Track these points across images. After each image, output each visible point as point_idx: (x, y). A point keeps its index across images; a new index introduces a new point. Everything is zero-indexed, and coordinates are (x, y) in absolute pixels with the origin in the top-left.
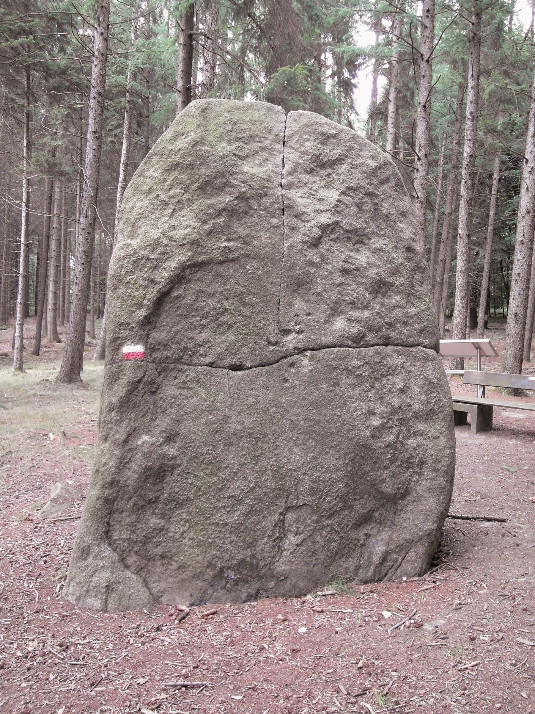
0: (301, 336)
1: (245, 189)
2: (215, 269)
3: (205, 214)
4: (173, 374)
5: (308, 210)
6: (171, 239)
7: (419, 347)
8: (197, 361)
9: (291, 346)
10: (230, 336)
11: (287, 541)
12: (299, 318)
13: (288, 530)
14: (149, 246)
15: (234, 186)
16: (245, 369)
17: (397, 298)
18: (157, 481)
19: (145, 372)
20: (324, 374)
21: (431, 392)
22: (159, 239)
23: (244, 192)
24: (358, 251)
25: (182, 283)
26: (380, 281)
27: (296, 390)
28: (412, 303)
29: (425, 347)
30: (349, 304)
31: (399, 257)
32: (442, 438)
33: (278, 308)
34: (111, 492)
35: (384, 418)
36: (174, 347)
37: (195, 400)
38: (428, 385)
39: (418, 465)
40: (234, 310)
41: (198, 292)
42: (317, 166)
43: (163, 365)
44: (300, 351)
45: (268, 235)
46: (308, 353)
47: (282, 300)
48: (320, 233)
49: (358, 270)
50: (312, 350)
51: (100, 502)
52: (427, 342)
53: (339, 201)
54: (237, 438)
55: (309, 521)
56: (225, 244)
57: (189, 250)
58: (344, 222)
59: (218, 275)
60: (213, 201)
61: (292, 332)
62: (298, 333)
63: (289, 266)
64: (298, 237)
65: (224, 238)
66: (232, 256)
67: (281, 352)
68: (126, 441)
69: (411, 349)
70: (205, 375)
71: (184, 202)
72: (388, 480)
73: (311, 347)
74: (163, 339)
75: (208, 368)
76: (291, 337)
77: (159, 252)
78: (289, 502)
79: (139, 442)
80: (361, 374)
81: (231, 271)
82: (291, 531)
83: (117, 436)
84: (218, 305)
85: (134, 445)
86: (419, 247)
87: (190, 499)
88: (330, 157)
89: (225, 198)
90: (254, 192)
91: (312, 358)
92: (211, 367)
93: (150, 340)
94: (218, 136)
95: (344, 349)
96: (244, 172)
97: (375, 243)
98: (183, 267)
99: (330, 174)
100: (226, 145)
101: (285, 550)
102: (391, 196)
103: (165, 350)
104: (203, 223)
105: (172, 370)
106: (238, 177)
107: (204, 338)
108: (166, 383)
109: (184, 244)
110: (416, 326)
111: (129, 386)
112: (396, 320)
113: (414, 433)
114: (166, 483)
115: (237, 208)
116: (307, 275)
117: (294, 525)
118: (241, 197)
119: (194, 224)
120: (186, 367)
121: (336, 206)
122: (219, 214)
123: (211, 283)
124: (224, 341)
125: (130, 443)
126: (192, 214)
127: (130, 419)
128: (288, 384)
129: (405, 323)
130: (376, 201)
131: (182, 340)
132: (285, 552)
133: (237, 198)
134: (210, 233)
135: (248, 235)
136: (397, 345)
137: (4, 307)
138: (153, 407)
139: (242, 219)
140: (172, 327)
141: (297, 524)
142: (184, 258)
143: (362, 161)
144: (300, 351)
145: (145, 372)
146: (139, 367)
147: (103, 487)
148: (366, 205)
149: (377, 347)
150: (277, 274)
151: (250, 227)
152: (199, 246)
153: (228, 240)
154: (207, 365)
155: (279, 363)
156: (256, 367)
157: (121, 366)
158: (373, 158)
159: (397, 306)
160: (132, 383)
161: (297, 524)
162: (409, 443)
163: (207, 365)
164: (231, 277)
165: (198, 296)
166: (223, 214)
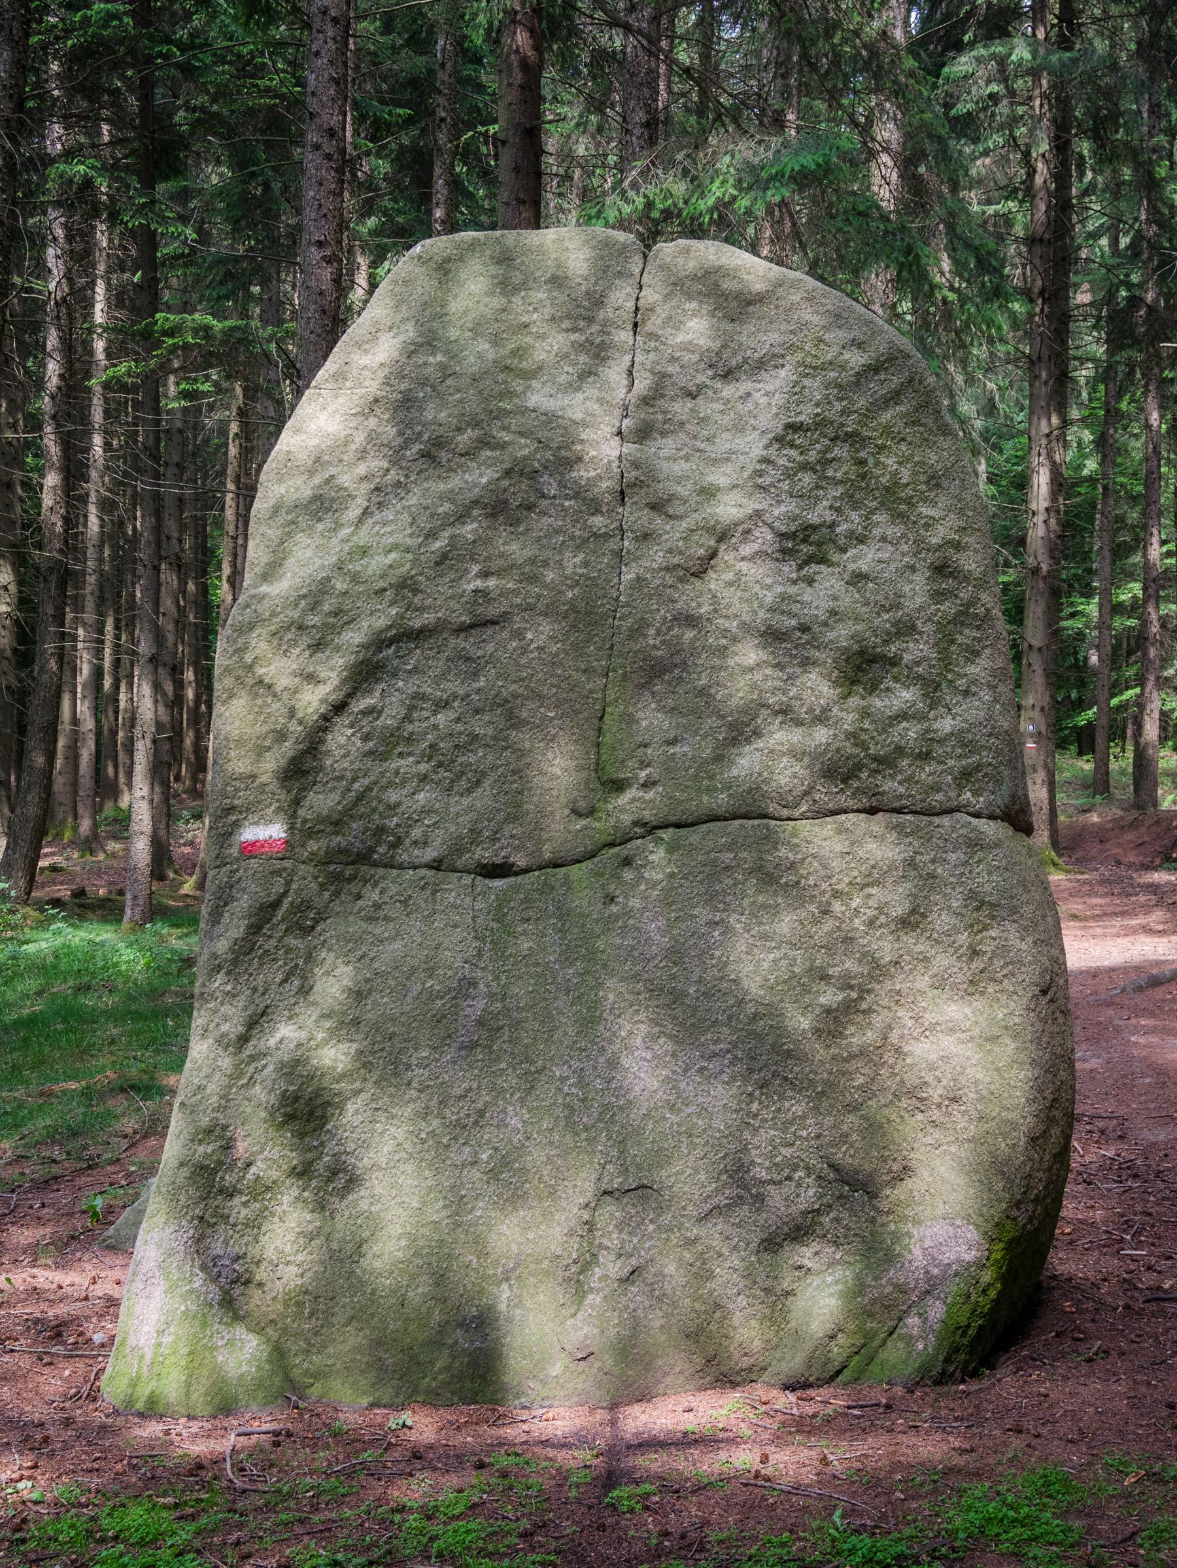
0: (650, 795)
1: (526, 452)
2: (452, 642)
3: (432, 515)
4: (354, 887)
5: (683, 490)
6: (355, 578)
7: (958, 815)
8: (405, 857)
9: (626, 819)
10: (482, 799)
11: (597, 1270)
12: (649, 751)
13: (601, 1246)
14: (304, 596)
15: (503, 446)
16: (516, 874)
17: (905, 696)
18: (309, 1128)
19: (288, 883)
20: (701, 882)
21: (985, 928)
22: (329, 579)
23: (525, 458)
24: (810, 582)
25: (377, 680)
26: (861, 653)
27: (631, 922)
28: (946, 706)
29: (977, 815)
30: (777, 713)
31: (916, 590)
32: (1008, 1041)
33: (600, 730)
34: (209, 1151)
35: (852, 987)
36: (354, 826)
37: (397, 945)
38: (978, 909)
39: (939, 1106)
40: (494, 738)
41: (413, 698)
42: (713, 378)
43: (332, 867)
44: (650, 829)
45: (581, 556)
46: (666, 834)
47: (608, 710)
48: (712, 543)
49: (804, 628)
50: (678, 826)
51: (185, 1172)
52: (980, 803)
53: (766, 460)
54: (489, 1030)
55: (651, 1227)
56: (479, 583)
57: (392, 603)
58: (776, 513)
59: (460, 658)
60: (455, 482)
61: (630, 786)
62: (645, 786)
63: (630, 629)
64: (656, 556)
65: (476, 569)
66: (492, 612)
67: (600, 831)
68: (244, 1039)
69: (937, 820)
70: (423, 888)
71: (389, 489)
72: (855, 1137)
73: (673, 819)
74: (331, 809)
75: (429, 873)
76: (631, 793)
77: (326, 608)
78: (606, 1180)
79: (272, 1042)
80: (798, 883)
81: (490, 647)
82: (607, 1248)
83: (225, 1028)
84: (459, 727)
85: (262, 1047)
86: (971, 562)
87: (380, 1168)
88: (749, 352)
89: (481, 475)
90: (549, 455)
91: (672, 849)
92: (438, 869)
93: (301, 812)
94: (470, 326)
95: (756, 822)
96: (527, 408)
97: (855, 559)
98: (380, 642)
99: (749, 394)
100: (487, 346)
101: (591, 1290)
102: (903, 440)
103: (336, 833)
104: (427, 537)
105: (349, 880)
106: (514, 422)
107: (421, 803)
108: (337, 909)
109: (385, 590)
110: (951, 762)
111: (250, 916)
112: (900, 751)
113: (933, 1027)
114: (328, 1131)
115: (507, 495)
116: (675, 648)
117: (615, 1236)
118: (518, 471)
119: (409, 541)
120: (381, 871)
121: (760, 473)
122: (461, 517)
123: (443, 676)
124: (470, 809)
125: (253, 1042)
126: (406, 518)
127: (255, 990)
128: (614, 909)
129: (925, 756)
130: (863, 454)
131: (374, 810)
132: (591, 1296)
133: (508, 473)
134: (443, 559)
135: (532, 561)
136: (898, 811)
137: (1172, 163)
138: (305, 963)
139: (517, 522)
140: (354, 780)
141: (620, 1232)
142: (381, 622)
143: (829, 357)
144: (650, 829)
145: (288, 883)
146: (278, 873)
147: (192, 1141)
148: (835, 465)
149: (843, 817)
150: (599, 649)
151: (539, 539)
152: (416, 591)
153: (485, 574)
154: (428, 866)
155: (596, 860)
156: (540, 868)
157: (238, 870)
158: (859, 345)
159: (903, 716)
160: (260, 909)
161: (620, 1232)
162: (918, 1052)
163: (428, 866)
164: (491, 659)
165: (412, 708)
166: (475, 512)
